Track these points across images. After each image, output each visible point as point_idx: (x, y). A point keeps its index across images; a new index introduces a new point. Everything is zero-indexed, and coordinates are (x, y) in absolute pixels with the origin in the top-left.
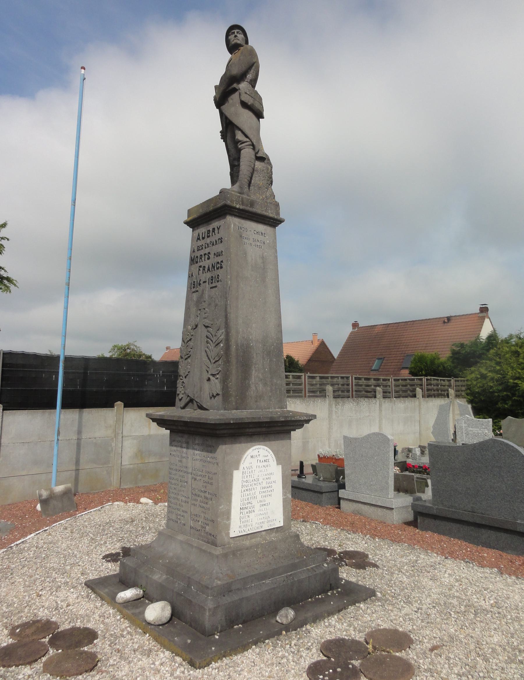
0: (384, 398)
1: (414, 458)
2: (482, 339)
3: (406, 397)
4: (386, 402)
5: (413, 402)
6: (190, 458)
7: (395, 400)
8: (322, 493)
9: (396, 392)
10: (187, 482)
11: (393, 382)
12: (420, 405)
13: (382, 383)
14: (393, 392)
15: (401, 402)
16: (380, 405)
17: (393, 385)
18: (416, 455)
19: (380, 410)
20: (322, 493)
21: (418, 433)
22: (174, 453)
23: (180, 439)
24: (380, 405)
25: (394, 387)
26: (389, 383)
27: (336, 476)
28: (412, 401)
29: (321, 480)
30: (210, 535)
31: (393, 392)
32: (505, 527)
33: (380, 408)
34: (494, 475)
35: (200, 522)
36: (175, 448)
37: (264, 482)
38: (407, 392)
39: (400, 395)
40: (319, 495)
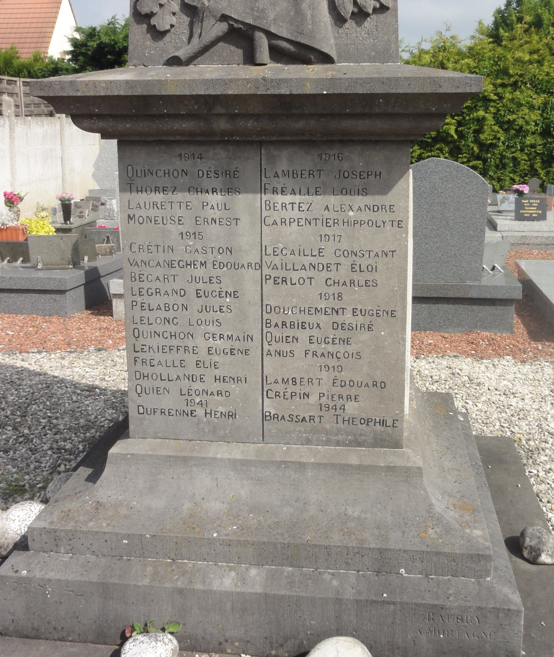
0: (16, 116)
1: (109, 216)
2: (118, 23)
3: (39, 115)
4: (19, 124)
5: (53, 125)
6: (245, 220)
7: (30, 121)
8: (62, 292)
9: (27, 106)
10: (235, 295)
11: (22, 87)
12: (62, 130)
13: (6, 89)
14: (23, 106)
15: (38, 124)
16: (11, 129)
17: (22, 92)
18: (113, 211)
19: (12, 137)
20: (62, 292)
21: (60, 179)
22: (143, 213)
23: (179, 164)
24: (11, 129)
25: (24, 96)
26: (17, 90)
27: (72, 258)
28: (51, 123)
29: (40, 270)
30: (367, 421)
31: (23, 106)
32: (450, 295)
33: (11, 136)
34: (433, 217)
35: (314, 398)
36: (143, 197)
37: (346, 263)
38: (39, 107)
39: (32, 112)
40: (58, 297)
